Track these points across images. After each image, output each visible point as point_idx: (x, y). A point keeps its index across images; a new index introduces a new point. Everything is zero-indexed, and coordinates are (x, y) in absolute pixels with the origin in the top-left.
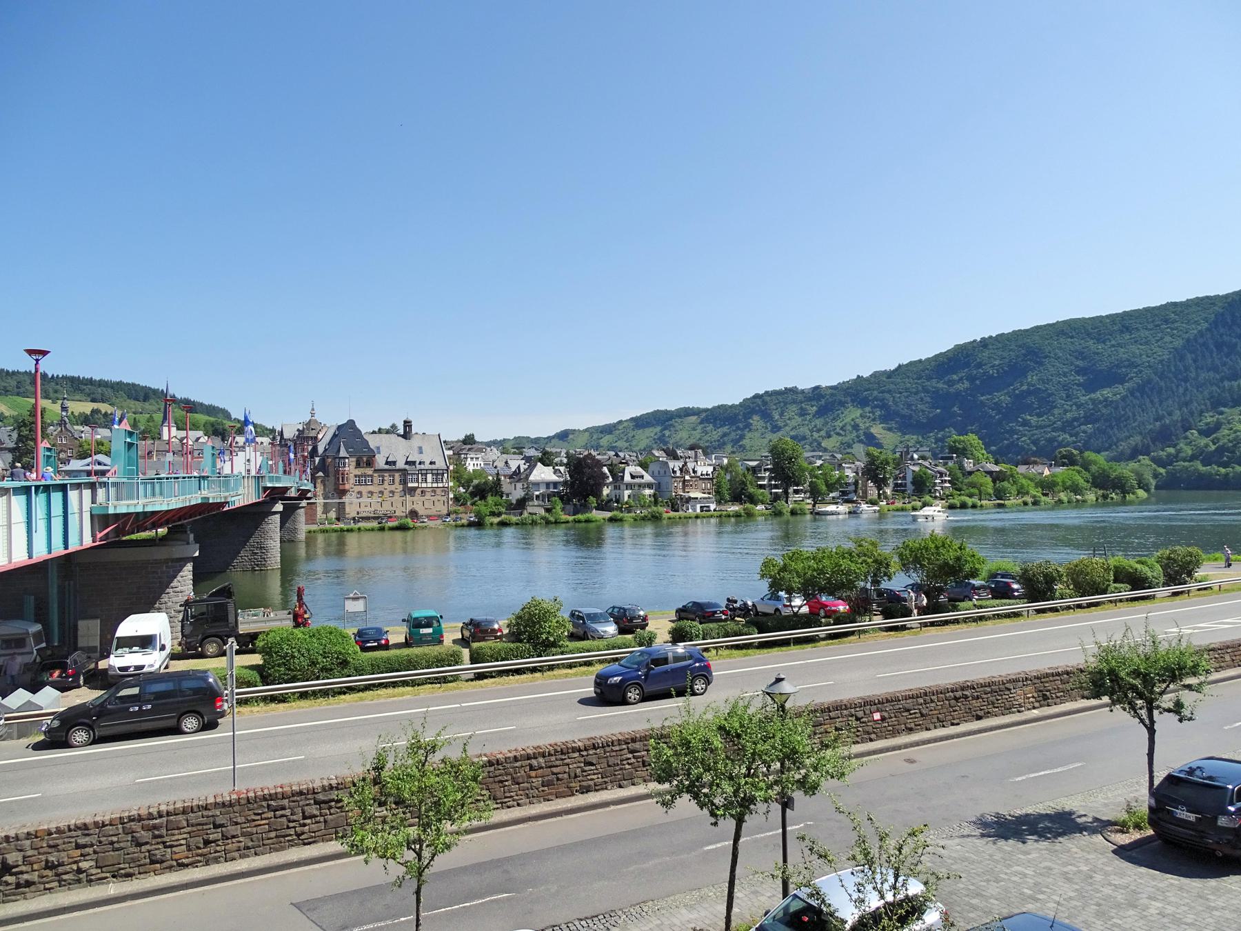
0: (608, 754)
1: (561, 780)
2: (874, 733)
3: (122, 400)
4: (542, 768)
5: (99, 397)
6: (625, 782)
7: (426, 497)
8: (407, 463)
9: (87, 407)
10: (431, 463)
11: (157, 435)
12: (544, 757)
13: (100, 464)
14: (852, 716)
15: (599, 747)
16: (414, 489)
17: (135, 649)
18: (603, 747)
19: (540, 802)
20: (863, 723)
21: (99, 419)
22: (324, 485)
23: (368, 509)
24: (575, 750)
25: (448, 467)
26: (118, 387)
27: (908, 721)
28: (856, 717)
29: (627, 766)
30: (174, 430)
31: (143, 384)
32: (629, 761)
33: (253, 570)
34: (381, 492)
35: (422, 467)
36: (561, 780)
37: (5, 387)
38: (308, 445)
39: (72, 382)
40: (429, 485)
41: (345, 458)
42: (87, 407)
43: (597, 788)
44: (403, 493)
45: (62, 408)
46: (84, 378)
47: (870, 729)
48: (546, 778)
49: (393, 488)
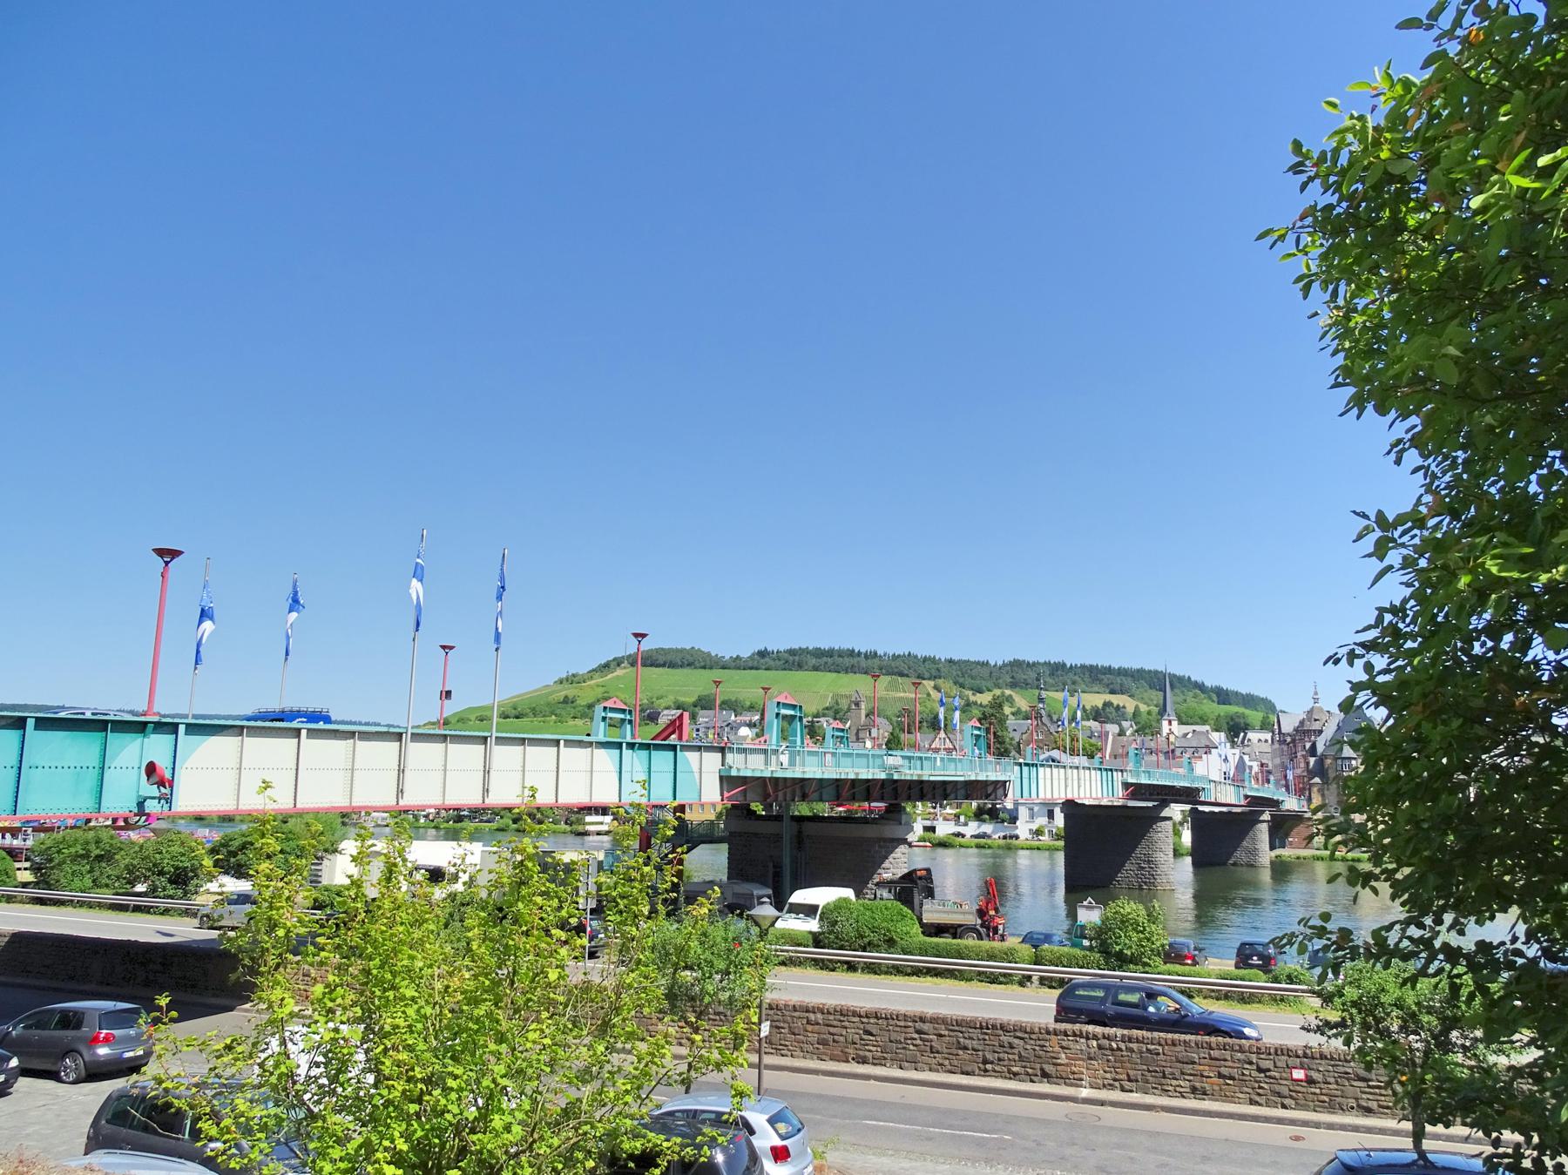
0: (891, 1028)
1: (837, 1042)
2: (1291, 1097)
3: (1142, 690)
4: (818, 1024)
5: (1117, 687)
6: (906, 1064)
9: (1096, 700)
12: (823, 1013)
14: (1251, 1063)
15: (882, 1018)
17: (801, 916)
18: (887, 1019)
19: (812, 1059)
20: (1270, 1077)
21: (1111, 713)
24: (855, 1014)
26: (1138, 675)
27: (1364, 1096)
28: (1258, 1066)
29: (911, 1047)
30: (1175, 723)
32: (914, 1042)
33: (1141, 888)
36: (837, 1042)
37: (1025, 680)
42: (1096, 700)
43: (875, 1061)
47: (1285, 1091)
48: (822, 1036)
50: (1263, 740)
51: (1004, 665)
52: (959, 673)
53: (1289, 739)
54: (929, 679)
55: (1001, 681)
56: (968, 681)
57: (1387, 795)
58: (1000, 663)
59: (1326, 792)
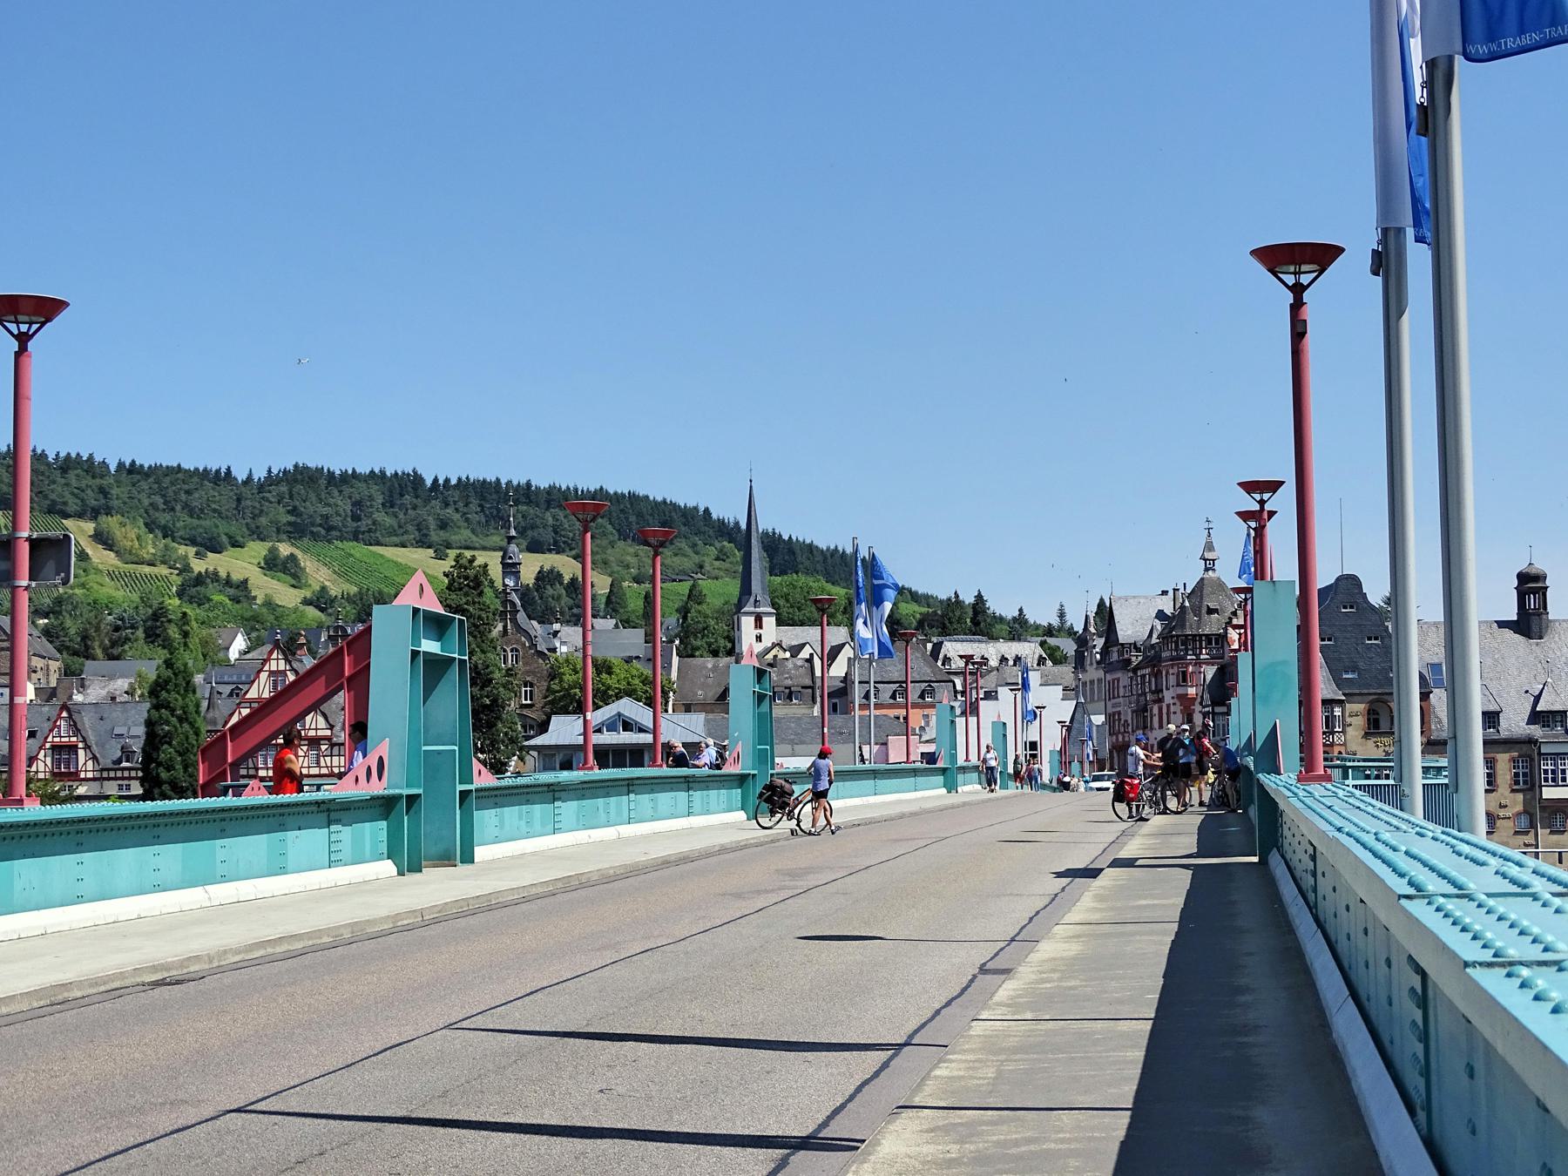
5: (547, 536)
8: (1536, 717)
11: (722, 642)
13: (628, 726)
21: (559, 598)
31: (657, 495)
37: (326, 517)
38: (1198, 663)
39: (483, 498)
44: (1524, 821)
45: (504, 565)
46: (509, 483)
50: (1011, 658)
51: (271, 480)
52: (159, 500)
54: (80, 515)
55: (263, 520)
56: (183, 521)
58: (260, 474)
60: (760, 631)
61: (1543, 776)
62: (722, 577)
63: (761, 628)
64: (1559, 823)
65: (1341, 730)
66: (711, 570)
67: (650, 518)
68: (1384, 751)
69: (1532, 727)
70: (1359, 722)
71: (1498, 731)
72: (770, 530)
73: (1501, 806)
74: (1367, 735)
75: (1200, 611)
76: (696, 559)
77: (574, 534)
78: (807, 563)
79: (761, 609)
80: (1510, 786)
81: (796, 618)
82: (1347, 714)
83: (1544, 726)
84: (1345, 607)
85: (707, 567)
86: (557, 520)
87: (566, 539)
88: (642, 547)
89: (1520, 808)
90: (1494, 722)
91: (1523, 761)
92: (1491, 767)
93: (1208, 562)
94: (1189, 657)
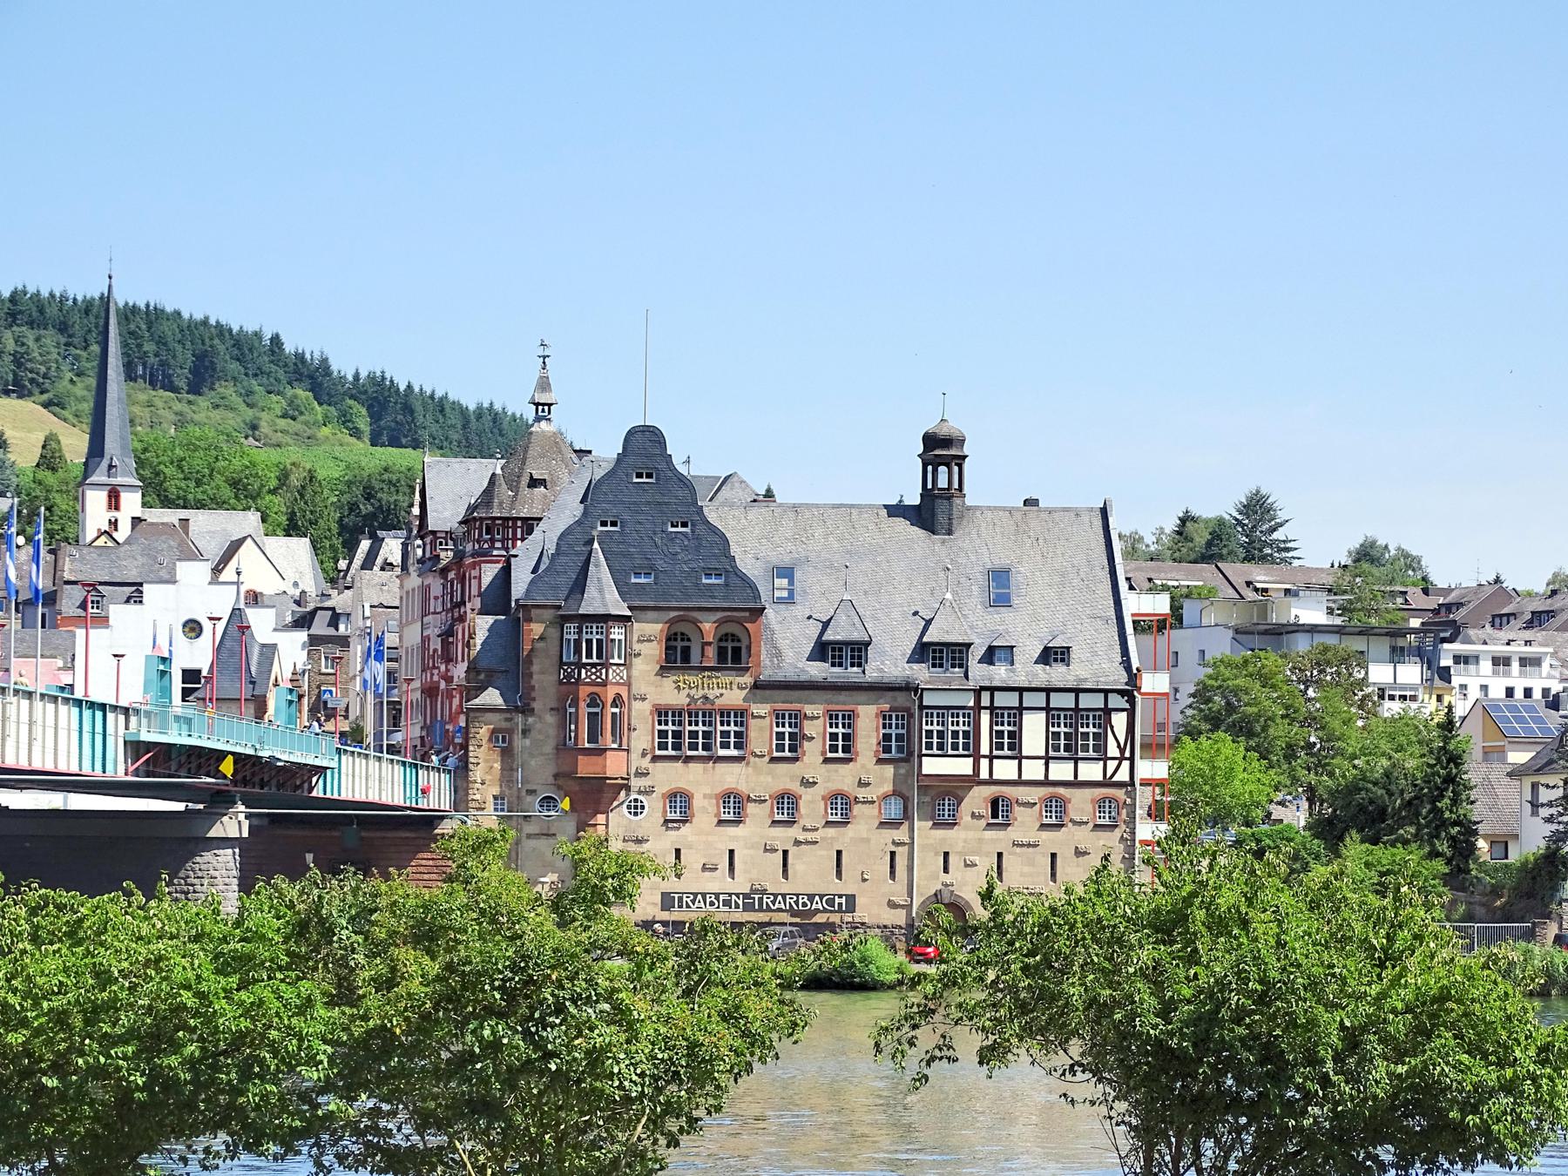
7: (1013, 833)
8: (925, 652)
10: (1051, 655)
16: (953, 788)
22: (507, 753)
23: (718, 883)
25: (1133, 678)
30: (132, 503)
31: (193, 310)
34: (787, 802)
35: (999, 673)
40: (1033, 770)
41: (606, 619)
44: (894, 809)
49: (843, 778)
53: (446, 556)
57: (1310, 829)
59: (519, 742)
60: (115, 514)
61: (924, 740)
62: (288, 445)
63: (117, 508)
64: (946, 813)
65: (622, 662)
66: (271, 434)
67: (179, 348)
68: (688, 695)
69: (915, 666)
70: (651, 653)
71: (864, 672)
72: (378, 374)
73: (861, 784)
74: (663, 670)
75: (519, 482)
76: (249, 414)
77: (49, 369)
78: (434, 428)
79: (119, 480)
80: (824, 753)
81: (190, 497)
82: (635, 638)
83: (934, 666)
84: (639, 475)
85: (265, 428)
86: (23, 344)
87: (35, 376)
88: (161, 392)
89: (888, 787)
90: (860, 657)
91: (897, 717)
92: (796, 723)
93: (540, 408)
94: (495, 553)
